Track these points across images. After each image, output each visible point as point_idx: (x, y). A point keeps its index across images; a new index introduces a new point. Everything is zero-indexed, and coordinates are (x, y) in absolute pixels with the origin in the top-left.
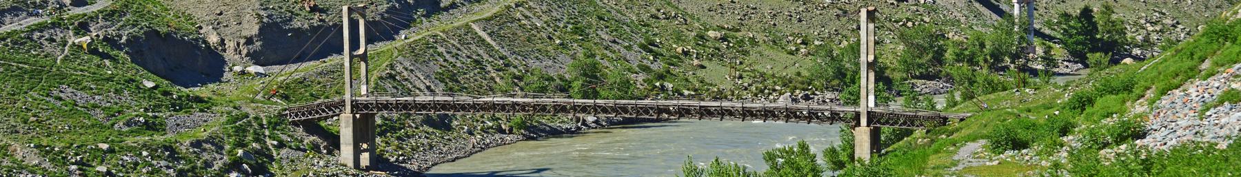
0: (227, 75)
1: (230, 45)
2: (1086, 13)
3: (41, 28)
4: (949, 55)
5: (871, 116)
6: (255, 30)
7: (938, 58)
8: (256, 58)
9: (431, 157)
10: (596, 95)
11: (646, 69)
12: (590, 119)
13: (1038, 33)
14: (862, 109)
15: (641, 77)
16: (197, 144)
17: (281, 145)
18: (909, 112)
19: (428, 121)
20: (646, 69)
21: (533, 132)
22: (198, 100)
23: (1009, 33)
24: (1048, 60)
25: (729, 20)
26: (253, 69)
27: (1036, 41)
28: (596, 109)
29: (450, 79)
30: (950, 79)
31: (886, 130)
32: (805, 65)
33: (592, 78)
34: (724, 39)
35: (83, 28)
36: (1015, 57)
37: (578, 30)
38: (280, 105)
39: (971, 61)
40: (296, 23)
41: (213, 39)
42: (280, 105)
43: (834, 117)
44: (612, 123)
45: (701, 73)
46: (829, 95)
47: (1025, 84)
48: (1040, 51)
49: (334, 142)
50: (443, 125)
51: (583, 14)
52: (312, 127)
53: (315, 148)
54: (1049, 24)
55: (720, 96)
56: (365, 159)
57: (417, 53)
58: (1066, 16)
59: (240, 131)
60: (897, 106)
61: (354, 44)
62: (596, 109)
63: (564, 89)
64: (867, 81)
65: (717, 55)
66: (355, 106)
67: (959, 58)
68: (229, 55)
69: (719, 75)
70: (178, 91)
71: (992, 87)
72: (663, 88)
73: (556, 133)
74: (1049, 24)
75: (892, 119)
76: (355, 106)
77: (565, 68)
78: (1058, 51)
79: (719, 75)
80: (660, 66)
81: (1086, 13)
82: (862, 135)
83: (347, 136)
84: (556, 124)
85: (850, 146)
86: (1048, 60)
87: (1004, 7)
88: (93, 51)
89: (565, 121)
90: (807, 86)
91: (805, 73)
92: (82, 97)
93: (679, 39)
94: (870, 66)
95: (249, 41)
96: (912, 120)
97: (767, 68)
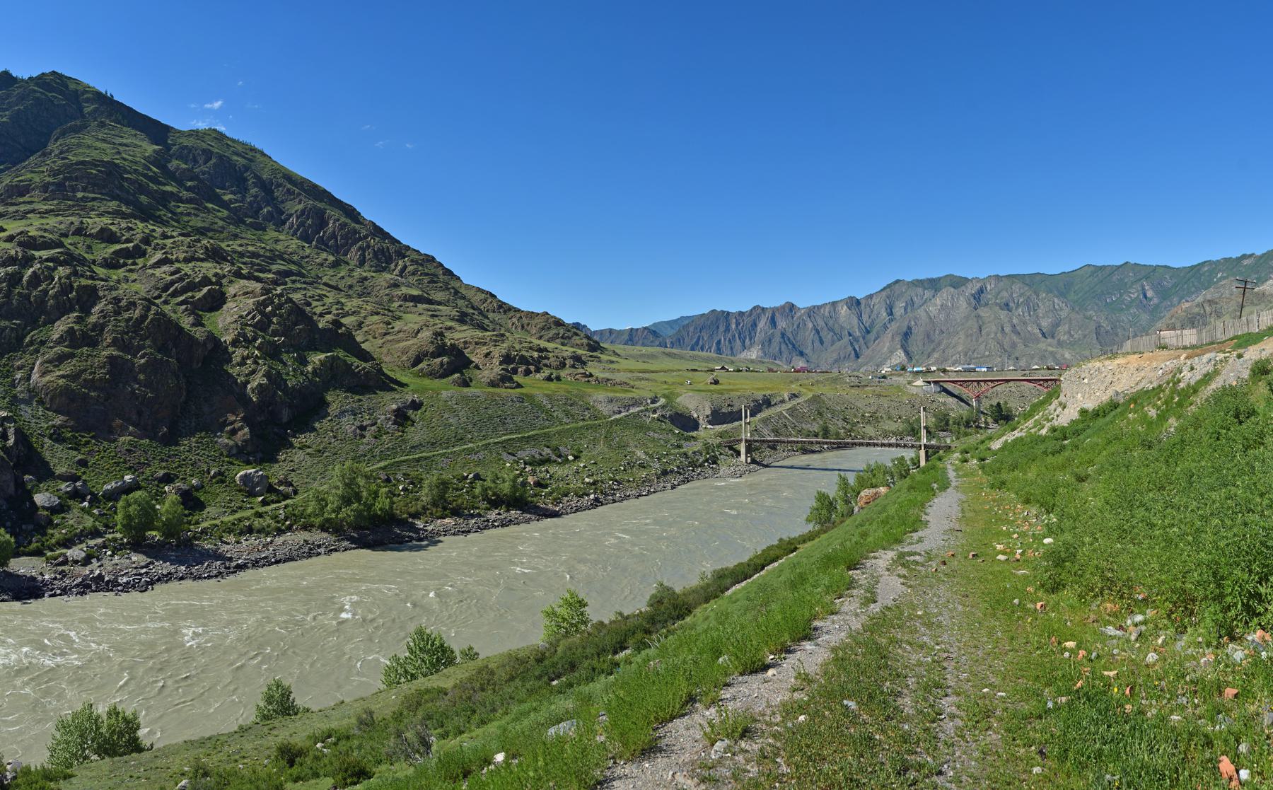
0: (700, 429)
1: (701, 418)
2: (999, 404)
3: (642, 411)
4: (951, 422)
5: (925, 446)
6: (709, 413)
7: (947, 424)
8: (710, 423)
9: (771, 460)
10: (827, 438)
11: (844, 428)
12: (825, 446)
13: (982, 413)
14: (922, 443)
15: (843, 431)
16: (694, 453)
17: (721, 454)
18: (938, 444)
19: (769, 447)
20: (844, 428)
21: (805, 451)
22: (693, 437)
23: (972, 413)
24: (986, 423)
25: (873, 409)
26: (709, 426)
27: (982, 416)
28: (826, 443)
29: (776, 431)
30: (951, 431)
31: (930, 451)
32: (899, 426)
33: (826, 432)
34: (871, 416)
35: (654, 411)
36: (974, 422)
37: (820, 414)
38: (719, 440)
39: (959, 424)
40: (723, 411)
41: (695, 416)
42: (719, 440)
43: (913, 446)
44: (833, 448)
45: (863, 429)
46: (909, 438)
47: (978, 433)
48: (983, 419)
49: (738, 454)
50: (774, 448)
51: (821, 407)
52: (731, 448)
53: (732, 455)
54: (986, 409)
55: (871, 438)
56: (749, 459)
57: (765, 421)
58: (992, 406)
59: (707, 448)
60: (933, 442)
61: (746, 417)
62: (826, 443)
63: (816, 436)
64: (923, 433)
65: (869, 422)
66: (746, 441)
67: (954, 423)
68: (701, 421)
69: (870, 430)
70: (686, 434)
71: (966, 434)
72: (850, 435)
73: (813, 452)
74: (986, 409)
75: (932, 447)
76: (746, 441)
77: (815, 427)
78: (990, 420)
79: (870, 430)
80: (848, 427)
81: (999, 404)
82: (922, 453)
83: (743, 450)
84: (813, 448)
85: (918, 457)
86: (986, 423)
87: (970, 402)
88: (658, 420)
89: (817, 448)
90: (900, 434)
91: (900, 429)
92: (656, 435)
93: (855, 416)
94: (924, 427)
95: (707, 416)
96: (939, 448)
97: (887, 428)
